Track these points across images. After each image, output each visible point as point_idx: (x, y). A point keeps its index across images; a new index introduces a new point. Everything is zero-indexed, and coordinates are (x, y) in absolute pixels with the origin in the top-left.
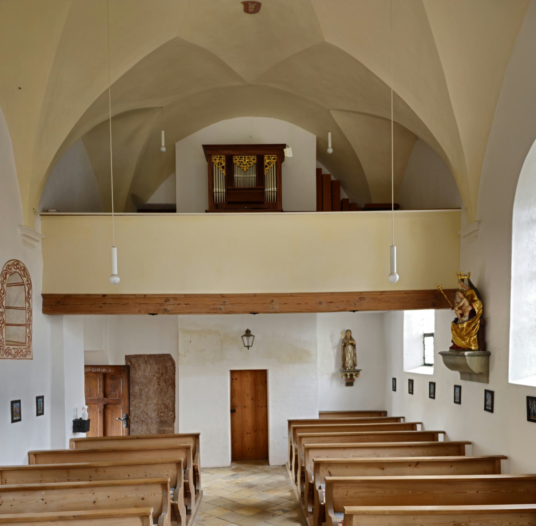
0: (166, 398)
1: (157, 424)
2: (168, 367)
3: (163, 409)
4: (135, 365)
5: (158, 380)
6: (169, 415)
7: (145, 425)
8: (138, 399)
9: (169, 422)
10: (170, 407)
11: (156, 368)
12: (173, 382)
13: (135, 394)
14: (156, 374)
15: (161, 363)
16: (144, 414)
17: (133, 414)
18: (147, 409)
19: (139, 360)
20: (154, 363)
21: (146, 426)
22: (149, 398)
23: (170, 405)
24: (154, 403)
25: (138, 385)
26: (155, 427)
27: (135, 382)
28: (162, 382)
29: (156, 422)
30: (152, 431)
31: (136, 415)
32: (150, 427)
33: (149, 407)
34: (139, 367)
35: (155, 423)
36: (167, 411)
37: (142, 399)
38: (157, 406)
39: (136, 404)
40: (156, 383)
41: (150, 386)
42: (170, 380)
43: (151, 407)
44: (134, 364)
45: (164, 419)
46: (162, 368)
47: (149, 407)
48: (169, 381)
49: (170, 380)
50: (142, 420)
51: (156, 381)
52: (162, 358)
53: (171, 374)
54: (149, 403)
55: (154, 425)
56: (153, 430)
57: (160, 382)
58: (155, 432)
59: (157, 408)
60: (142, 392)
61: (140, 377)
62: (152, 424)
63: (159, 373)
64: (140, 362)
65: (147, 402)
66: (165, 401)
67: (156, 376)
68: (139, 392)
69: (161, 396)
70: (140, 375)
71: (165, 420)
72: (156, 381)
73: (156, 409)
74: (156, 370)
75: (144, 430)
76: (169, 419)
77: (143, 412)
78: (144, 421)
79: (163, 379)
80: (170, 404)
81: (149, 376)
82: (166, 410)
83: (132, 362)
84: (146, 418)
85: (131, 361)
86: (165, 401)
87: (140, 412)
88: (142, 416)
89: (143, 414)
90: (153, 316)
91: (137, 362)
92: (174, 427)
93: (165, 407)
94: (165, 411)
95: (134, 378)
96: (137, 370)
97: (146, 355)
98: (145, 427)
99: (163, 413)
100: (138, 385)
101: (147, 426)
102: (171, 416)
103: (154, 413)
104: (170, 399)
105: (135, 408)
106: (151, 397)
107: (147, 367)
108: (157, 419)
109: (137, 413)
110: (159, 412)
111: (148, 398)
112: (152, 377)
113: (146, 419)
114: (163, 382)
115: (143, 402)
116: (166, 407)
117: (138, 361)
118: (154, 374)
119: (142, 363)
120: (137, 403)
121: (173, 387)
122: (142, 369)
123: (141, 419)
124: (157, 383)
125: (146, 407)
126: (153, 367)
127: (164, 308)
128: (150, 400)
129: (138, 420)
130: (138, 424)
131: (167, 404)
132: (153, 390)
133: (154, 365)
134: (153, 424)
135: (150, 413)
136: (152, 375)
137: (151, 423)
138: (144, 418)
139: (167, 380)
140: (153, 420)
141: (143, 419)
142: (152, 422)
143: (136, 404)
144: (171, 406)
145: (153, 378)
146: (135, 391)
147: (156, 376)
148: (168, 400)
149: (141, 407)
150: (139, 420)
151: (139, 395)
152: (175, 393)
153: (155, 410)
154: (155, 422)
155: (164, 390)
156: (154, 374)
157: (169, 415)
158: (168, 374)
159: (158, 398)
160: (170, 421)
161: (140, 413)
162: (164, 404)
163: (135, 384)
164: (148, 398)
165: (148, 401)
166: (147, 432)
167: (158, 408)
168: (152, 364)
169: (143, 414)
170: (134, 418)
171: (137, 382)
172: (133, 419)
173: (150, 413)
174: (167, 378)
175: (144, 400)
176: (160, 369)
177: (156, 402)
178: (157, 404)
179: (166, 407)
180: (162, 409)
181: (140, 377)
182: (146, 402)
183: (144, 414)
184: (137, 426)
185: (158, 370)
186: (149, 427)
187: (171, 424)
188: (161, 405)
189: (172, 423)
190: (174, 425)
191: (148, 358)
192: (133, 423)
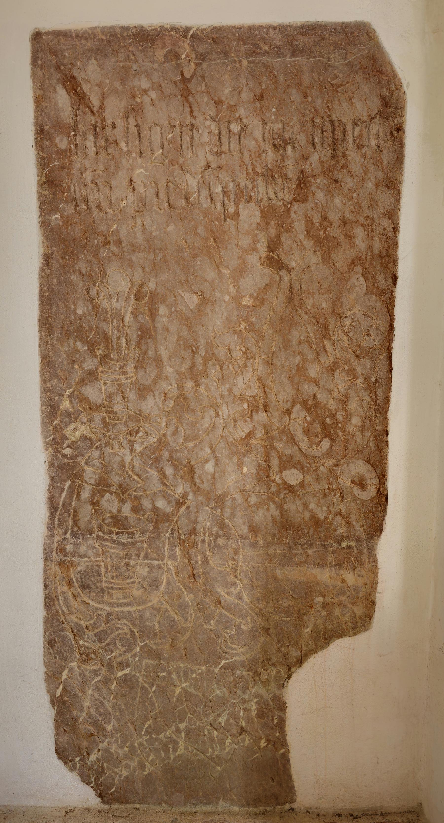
0: (327, 361)
1: (254, 545)
2: (349, 126)
3: (304, 443)
4: (102, 107)
5: (272, 232)
6: (346, 482)
7: (172, 546)
8: (130, 369)
9: (342, 530)
10: (351, 429)
11: (258, 134)
12: (377, 244)
13: (109, 328)
14: (260, 181)
15: (295, 95)
16: (169, 471)
17: (89, 470)
18: (186, 439)
19: (137, 74)
20: (245, 96)
21: (178, 552)
22: (206, 361)
23: (348, 415)
24: (242, 399)
25: (131, 264)
26: (240, 559)
27: (107, 243)
28: (301, 246)
29: (254, 529)
30: (221, 591)
31: (115, 479)
32: (206, 561)
33: (206, 423)
34: (132, 121)
35: (242, 537)
36: (329, 453)
37: (158, 361)
38: (261, 416)
39: (110, 397)
40: (255, 249)
41: (211, 274)
42: (359, 232)
43: (220, 422)
44: (95, 102)
45: (306, 506)
46: (302, 139)
47: (206, 423)
48: (350, 237)
49: (359, 232)
50: (155, 509)
51: (255, 242)
52: (300, 60)
53: (370, 185)
54: (202, 389)
55: (236, 552)
56: (227, 585)
57: (286, 239)
58: (240, 598)
59: (260, 433)
60: (153, 314)
61: (143, 201)
62: (221, 541)
63: (285, 177)
64: (145, 84)
65: (189, 384)
66: (316, 382)
67: (259, 202)
68: (135, 314)
69: (287, 344)
70: (141, 190)
71: (313, 516)
72: (255, 242)
73: (250, 435)
74: (260, 152)
75: (168, 582)
76: (339, 514)
77: (166, 454)
78: (167, 517)
79: (309, 220)
80: (353, 405)
81: (204, 193)
82: (326, 443)
83: (86, 87)
84: (185, 496)
85: (79, 75)
86: (316, 382)
87: (142, 454)
88: (157, 486)
89: (161, 471)
90: (55, 756)
91: (117, 84)
92: (374, 571)
93: (318, 428)
94: (315, 451)
95: (100, 208)
96: (123, 145)
97: (187, 30)
98: (173, 557)
99: (300, 466)
100: (131, 264)
101: (186, 554)
102: (357, 491)
103: (240, 466)
104: (351, 372)
105: (106, 425)
106: (221, 352)
107: (192, 127)
108: (259, 505)
109: (122, 465)
110: (275, 462)
111: (199, 362)
112: (232, 210)
113: (180, 504)
114: (309, 244)
115: (164, 386)
116: (324, 424)
117: (123, 81)
118: (244, 182)
119: (153, 95)
120: (121, 390)
121: (382, 282)
122: (157, 142)
123: (147, 504)
124: (262, 247)
125: (179, 419)
126: (235, 128)
127: (141, 124)
128: (214, 371)
129: (127, 509)
130: (125, 539)
131: (332, 405)
132: (237, 299)
133: (242, 112)
134: (232, 544)
135: (210, 467)
136: (225, 192)
137: (217, 536)
138: (165, 496)
139: (335, 232)
140: (233, 515)
141: (161, 504)
142: (222, 525)
143: (110, 397)
144: (356, 421)
145: (237, 214)
146: (106, 305)
147: (259, 202)
148: (338, 374)
149: (147, 418)
150: (135, 509)
151: (134, 337)
152: (391, 328)
153: (244, 523)
154: (244, 530)
155: (309, 303)
156: (244, 182)
157: (346, 482)
158: (349, 183)
159: (268, 364)
160: (348, 523)
161: (137, 463)
162: (305, 404)
163: (104, 253)
164: (199, 362)
165: (197, 384)
166: (188, 597)
167: (267, 429)
168: (232, 108)
169: (161, 471)
170: (101, 493)
171: (119, 243)
172: (94, 503)
173: (210, 467)
174: (334, 217)
175: (168, 370)
176: (286, 143)
177: (255, 391)
178: (262, 402)
179: (324, 424)
180: (293, 440)
181: (143, 201)
182: (181, 388)
183: (169, 471)
184: (115, 551)
185: (270, 155)
186: (199, 559)
187: (353, 544)
188: (288, 412)
189: (358, 540)
190: (372, 551)
191: (202, 57)
192: (91, 532)
